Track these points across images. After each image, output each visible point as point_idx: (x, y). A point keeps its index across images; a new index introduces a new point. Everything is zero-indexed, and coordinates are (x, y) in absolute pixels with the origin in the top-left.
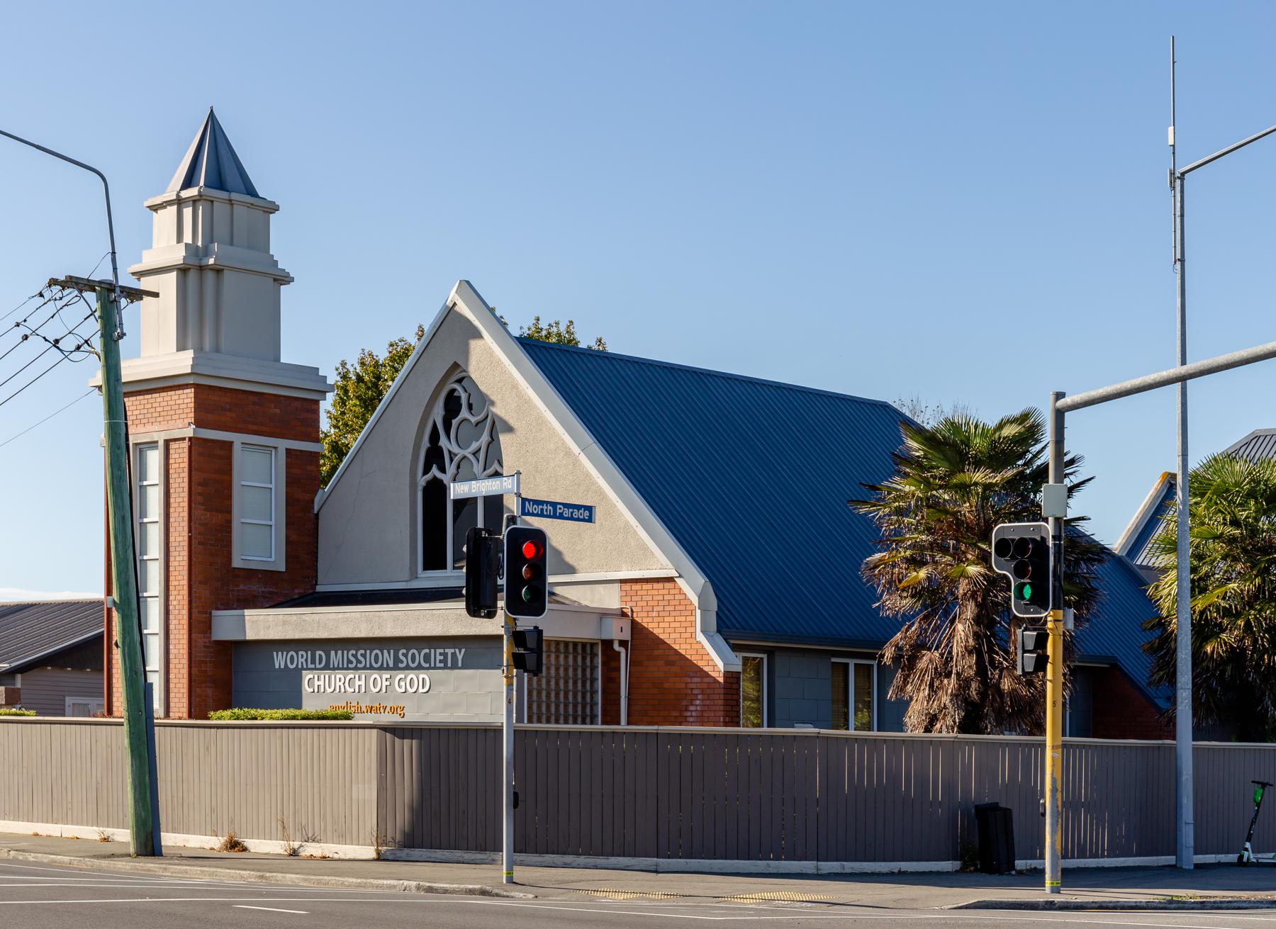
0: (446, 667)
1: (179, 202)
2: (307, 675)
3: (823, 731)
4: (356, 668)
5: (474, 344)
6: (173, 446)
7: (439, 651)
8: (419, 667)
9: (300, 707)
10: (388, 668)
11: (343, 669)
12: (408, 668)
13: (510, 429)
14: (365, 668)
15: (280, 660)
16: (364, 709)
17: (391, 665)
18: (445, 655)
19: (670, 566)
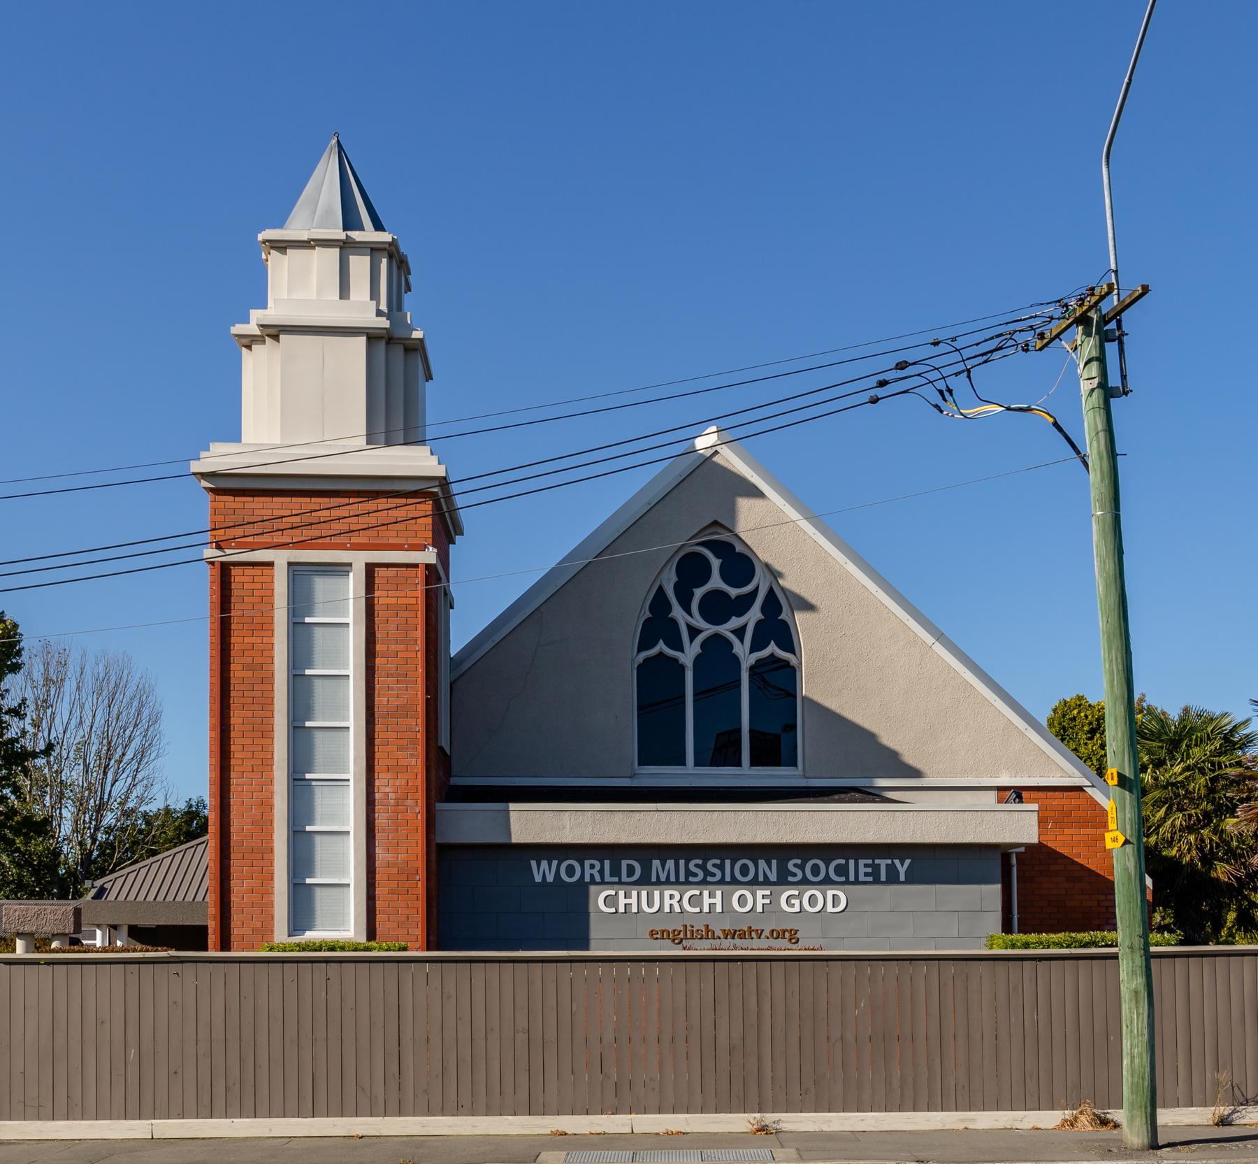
0: (877, 881)
1: (346, 247)
2: (600, 899)
3: (1015, 869)
4: (704, 882)
5: (744, 504)
6: (380, 573)
7: (862, 862)
8: (827, 881)
9: (585, 944)
10: (767, 882)
11: (677, 882)
12: (805, 882)
13: (809, 607)
14: (722, 882)
15: (543, 871)
16: (719, 933)
17: (773, 877)
18: (876, 868)
19: (1077, 773)
